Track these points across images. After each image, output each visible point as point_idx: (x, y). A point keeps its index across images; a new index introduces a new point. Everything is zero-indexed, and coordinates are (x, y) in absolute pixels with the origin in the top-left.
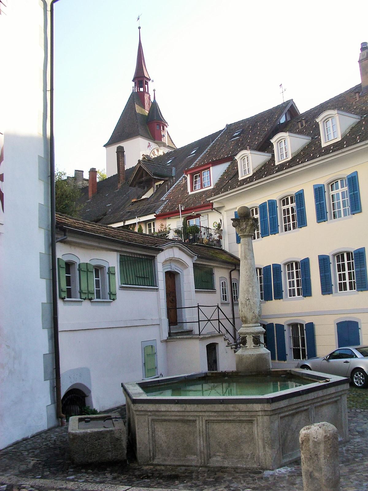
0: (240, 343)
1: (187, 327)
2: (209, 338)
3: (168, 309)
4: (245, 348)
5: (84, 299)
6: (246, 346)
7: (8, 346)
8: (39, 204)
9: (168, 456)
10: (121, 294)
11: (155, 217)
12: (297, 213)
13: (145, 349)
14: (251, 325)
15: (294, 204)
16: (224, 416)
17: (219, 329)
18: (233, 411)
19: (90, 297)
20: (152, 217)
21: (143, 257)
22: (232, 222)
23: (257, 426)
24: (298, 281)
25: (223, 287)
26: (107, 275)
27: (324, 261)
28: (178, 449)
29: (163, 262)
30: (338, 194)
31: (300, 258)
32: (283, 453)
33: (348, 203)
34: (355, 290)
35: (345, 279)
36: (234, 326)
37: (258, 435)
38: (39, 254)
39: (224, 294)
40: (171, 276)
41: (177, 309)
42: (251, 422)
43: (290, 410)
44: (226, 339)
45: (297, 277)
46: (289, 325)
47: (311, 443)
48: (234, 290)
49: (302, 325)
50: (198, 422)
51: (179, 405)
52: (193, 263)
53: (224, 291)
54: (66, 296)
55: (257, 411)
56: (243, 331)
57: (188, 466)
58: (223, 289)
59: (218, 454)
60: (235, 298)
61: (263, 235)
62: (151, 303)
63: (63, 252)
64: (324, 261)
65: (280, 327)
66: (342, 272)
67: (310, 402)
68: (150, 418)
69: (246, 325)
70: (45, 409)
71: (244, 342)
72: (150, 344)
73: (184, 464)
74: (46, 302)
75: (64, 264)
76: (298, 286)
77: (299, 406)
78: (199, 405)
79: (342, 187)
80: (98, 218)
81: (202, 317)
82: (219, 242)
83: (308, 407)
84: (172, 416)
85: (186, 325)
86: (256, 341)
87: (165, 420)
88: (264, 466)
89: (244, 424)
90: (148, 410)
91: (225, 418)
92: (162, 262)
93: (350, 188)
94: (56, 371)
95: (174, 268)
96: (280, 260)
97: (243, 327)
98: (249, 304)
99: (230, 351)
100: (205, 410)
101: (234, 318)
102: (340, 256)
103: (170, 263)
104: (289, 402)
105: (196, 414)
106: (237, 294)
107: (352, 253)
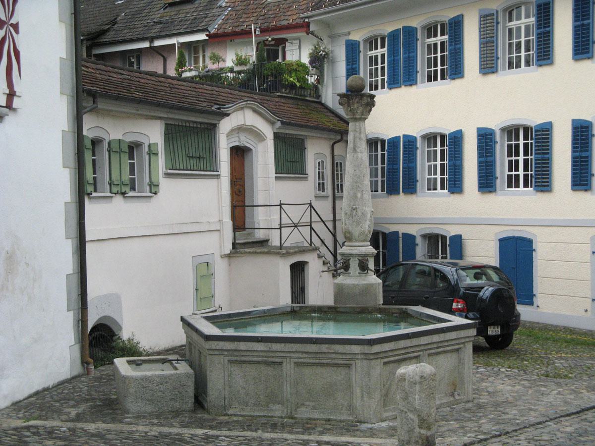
0: (340, 268)
1: (260, 235)
2: (295, 253)
3: (234, 207)
4: (347, 275)
5: (115, 194)
6: (349, 272)
7: (27, 264)
8: (60, 58)
9: (247, 405)
10: (165, 185)
11: (207, 38)
12: (450, 54)
13: (197, 268)
14: (357, 244)
15: (446, 38)
16: (316, 358)
17: (311, 240)
18: (328, 353)
19: (123, 191)
20: (202, 37)
21: (199, 126)
22: (339, 98)
23: (355, 371)
24: (442, 166)
25: (319, 169)
26: (147, 157)
27: (485, 138)
28: (259, 397)
29: (229, 133)
30: (519, 29)
31: (448, 129)
32: (385, 405)
33: (534, 46)
34: (532, 189)
35: (517, 169)
36: (334, 235)
37: (356, 382)
38: (61, 131)
39: (321, 182)
40: (239, 153)
41: (246, 208)
42: (348, 366)
43: (395, 355)
44: (321, 255)
45: (442, 159)
46: (424, 236)
47: (406, 383)
48: (337, 174)
49: (444, 238)
50: (284, 364)
51: (263, 344)
52: (274, 133)
53: (321, 176)
54: (93, 190)
55: (355, 354)
56: (346, 252)
57: (272, 417)
58: (319, 173)
59: (307, 403)
60: (337, 188)
61: (391, 84)
62: (209, 196)
63: (91, 127)
64: (485, 138)
65: (409, 239)
66: (513, 158)
67: (423, 348)
68: (227, 358)
69: (350, 244)
70: (68, 350)
71: (346, 267)
72: (205, 259)
73: (266, 415)
74: (70, 201)
75: (90, 142)
76: (442, 173)
77: (407, 351)
78: (287, 345)
79: (527, 16)
80: (102, 27)
81: (285, 220)
82: (316, 88)
83: (419, 353)
84: (253, 356)
85: (260, 231)
86: (363, 267)
87: (244, 362)
88: (362, 419)
89: (340, 369)
90: (225, 349)
91: (317, 361)
92: (226, 133)
93: (538, 21)
94: (81, 297)
95: (244, 140)
96: (416, 130)
97: (347, 246)
98: (355, 216)
99: (328, 276)
100: (294, 350)
101: (334, 221)
102: (512, 131)
103: (238, 133)
104: (394, 345)
105: (282, 354)
106: (342, 181)
107: (532, 128)
